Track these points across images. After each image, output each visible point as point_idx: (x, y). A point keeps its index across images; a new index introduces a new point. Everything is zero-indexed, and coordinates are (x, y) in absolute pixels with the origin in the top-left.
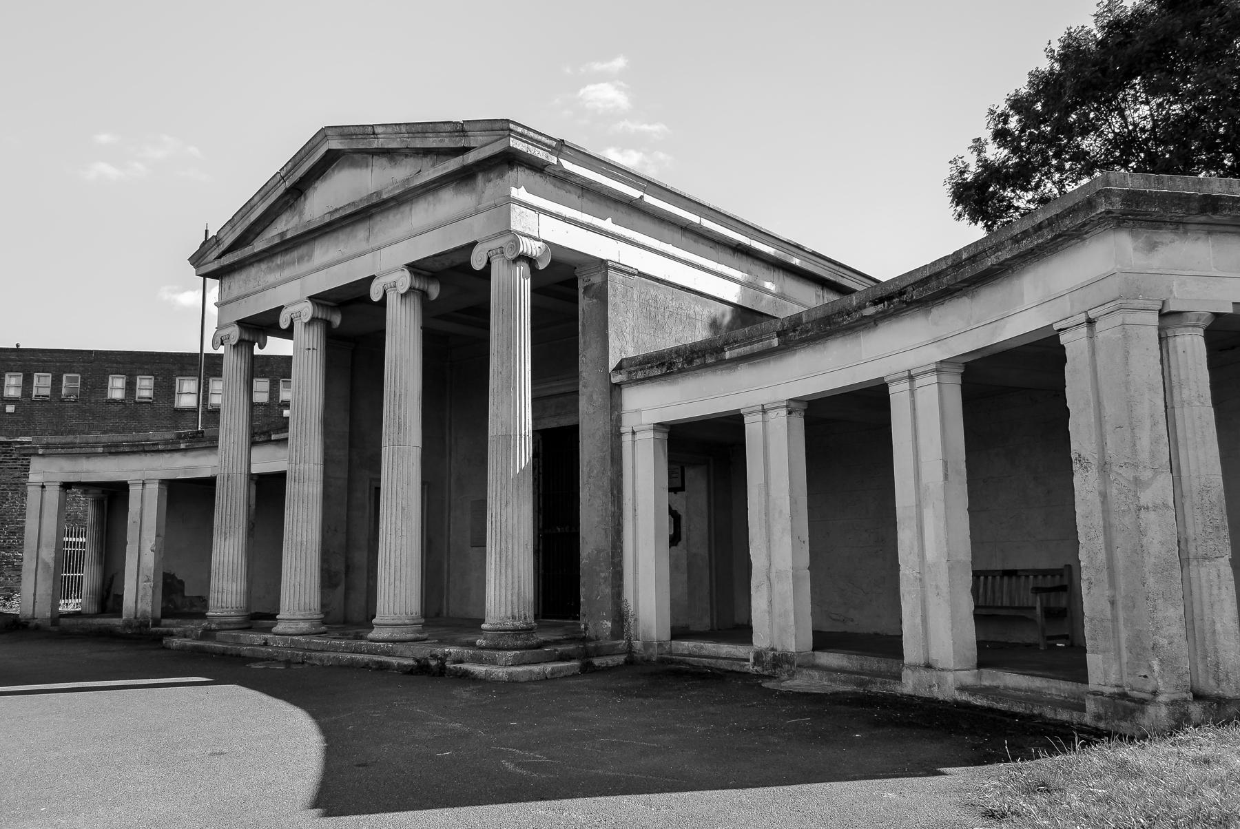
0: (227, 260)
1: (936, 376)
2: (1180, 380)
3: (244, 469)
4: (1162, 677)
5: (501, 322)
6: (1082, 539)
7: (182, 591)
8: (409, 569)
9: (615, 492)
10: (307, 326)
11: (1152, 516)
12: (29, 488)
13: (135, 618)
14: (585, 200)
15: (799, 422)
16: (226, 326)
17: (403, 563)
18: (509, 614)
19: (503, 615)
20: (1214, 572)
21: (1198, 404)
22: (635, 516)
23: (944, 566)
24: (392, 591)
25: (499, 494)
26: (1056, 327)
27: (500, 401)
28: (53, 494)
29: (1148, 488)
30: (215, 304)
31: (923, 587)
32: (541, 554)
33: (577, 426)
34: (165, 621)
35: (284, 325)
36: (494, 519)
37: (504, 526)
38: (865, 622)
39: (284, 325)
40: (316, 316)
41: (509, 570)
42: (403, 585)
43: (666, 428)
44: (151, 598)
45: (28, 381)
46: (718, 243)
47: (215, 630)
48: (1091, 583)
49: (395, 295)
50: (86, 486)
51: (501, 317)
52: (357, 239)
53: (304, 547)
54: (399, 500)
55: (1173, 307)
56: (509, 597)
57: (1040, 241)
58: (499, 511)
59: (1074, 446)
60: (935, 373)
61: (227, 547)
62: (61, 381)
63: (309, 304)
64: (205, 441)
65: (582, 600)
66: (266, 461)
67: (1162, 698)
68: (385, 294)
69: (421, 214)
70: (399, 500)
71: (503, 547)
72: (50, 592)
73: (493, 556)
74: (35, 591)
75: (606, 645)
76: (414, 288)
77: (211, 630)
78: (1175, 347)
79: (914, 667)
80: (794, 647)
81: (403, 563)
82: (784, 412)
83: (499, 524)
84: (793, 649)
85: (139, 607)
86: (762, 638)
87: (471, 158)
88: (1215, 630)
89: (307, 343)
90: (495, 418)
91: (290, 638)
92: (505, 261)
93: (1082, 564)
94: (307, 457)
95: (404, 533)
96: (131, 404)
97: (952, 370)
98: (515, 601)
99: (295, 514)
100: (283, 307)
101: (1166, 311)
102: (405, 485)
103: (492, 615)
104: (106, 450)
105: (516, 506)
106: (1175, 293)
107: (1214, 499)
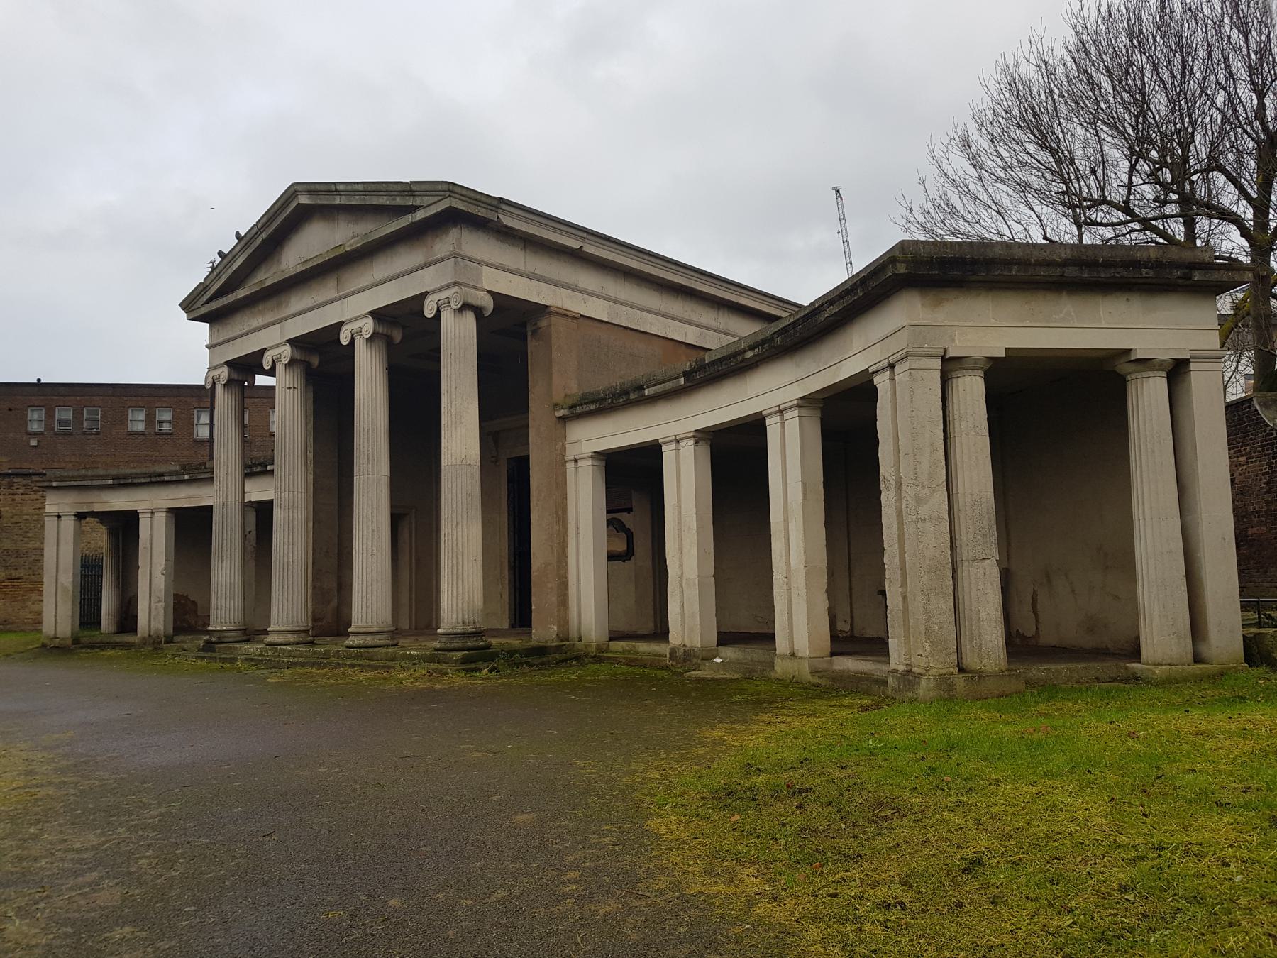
0: (214, 305)
1: (797, 411)
2: (960, 413)
3: (238, 498)
4: (932, 656)
5: (449, 366)
6: (886, 546)
7: (195, 612)
8: (380, 584)
9: (560, 513)
10: (287, 367)
11: (928, 526)
12: (46, 519)
13: (149, 635)
14: (527, 251)
15: (705, 452)
16: (216, 367)
17: (375, 578)
18: (460, 620)
19: (454, 620)
20: (981, 571)
21: (974, 433)
22: (578, 533)
23: (803, 571)
24: (364, 604)
25: (450, 517)
26: (871, 370)
27: (449, 435)
28: (69, 524)
29: (926, 504)
30: (207, 346)
31: (789, 589)
32: (517, 569)
33: (529, 456)
34: (176, 638)
35: (267, 367)
36: (446, 539)
37: (455, 545)
38: (744, 621)
39: (267, 367)
40: (295, 357)
41: (460, 582)
42: (374, 598)
43: (604, 456)
44: (163, 617)
45: (50, 414)
46: (662, 286)
47: (215, 643)
48: (891, 582)
49: (361, 339)
50: (104, 517)
51: (449, 361)
52: (327, 290)
53: (290, 567)
54: (370, 523)
55: (951, 354)
56: (460, 606)
57: (856, 298)
58: (450, 531)
59: (881, 471)
60: (797, 408)
61: (224, 569)
62: (82, 414)
63: (288, 348)
64: (201, 473)
65: (533, 608)
66: (258, 491)
67: (932, 672)
68: (439, 311)
69: (381, 268)
70: (370, 523)
71: (455, 562)
72: (70, 613)
73: (446, 571)
74: (56, 613)
75: (551, 647)
76: (378, 333)
77: (212, 643)
78: (957, 386)
79: (783, 657)
80: (699, 644)
81: (375, 578)
82: (691, 442)
83: (450, 543)
84: (699, 645)
85: (152, 626)
86: (675, 638)
87: (420, 215)
88: (979, 618)
89: (287, 383)
90: (446, 450)
91: (279, 647)
92: (452, 310)
93: (886, 566)
94: (291, 486)
95: (375, 552)
96: (153, 436)
97: (810, 405)
98: (466, 608)
99: (282, 538)
100: (265, 349)
101: (947, 356)
102: (375, 510)
103: (446, 621)
104: (116, 482)
105: (465, 526)
106: (957, 342)
107: (984, 511)
